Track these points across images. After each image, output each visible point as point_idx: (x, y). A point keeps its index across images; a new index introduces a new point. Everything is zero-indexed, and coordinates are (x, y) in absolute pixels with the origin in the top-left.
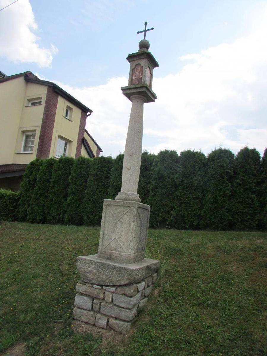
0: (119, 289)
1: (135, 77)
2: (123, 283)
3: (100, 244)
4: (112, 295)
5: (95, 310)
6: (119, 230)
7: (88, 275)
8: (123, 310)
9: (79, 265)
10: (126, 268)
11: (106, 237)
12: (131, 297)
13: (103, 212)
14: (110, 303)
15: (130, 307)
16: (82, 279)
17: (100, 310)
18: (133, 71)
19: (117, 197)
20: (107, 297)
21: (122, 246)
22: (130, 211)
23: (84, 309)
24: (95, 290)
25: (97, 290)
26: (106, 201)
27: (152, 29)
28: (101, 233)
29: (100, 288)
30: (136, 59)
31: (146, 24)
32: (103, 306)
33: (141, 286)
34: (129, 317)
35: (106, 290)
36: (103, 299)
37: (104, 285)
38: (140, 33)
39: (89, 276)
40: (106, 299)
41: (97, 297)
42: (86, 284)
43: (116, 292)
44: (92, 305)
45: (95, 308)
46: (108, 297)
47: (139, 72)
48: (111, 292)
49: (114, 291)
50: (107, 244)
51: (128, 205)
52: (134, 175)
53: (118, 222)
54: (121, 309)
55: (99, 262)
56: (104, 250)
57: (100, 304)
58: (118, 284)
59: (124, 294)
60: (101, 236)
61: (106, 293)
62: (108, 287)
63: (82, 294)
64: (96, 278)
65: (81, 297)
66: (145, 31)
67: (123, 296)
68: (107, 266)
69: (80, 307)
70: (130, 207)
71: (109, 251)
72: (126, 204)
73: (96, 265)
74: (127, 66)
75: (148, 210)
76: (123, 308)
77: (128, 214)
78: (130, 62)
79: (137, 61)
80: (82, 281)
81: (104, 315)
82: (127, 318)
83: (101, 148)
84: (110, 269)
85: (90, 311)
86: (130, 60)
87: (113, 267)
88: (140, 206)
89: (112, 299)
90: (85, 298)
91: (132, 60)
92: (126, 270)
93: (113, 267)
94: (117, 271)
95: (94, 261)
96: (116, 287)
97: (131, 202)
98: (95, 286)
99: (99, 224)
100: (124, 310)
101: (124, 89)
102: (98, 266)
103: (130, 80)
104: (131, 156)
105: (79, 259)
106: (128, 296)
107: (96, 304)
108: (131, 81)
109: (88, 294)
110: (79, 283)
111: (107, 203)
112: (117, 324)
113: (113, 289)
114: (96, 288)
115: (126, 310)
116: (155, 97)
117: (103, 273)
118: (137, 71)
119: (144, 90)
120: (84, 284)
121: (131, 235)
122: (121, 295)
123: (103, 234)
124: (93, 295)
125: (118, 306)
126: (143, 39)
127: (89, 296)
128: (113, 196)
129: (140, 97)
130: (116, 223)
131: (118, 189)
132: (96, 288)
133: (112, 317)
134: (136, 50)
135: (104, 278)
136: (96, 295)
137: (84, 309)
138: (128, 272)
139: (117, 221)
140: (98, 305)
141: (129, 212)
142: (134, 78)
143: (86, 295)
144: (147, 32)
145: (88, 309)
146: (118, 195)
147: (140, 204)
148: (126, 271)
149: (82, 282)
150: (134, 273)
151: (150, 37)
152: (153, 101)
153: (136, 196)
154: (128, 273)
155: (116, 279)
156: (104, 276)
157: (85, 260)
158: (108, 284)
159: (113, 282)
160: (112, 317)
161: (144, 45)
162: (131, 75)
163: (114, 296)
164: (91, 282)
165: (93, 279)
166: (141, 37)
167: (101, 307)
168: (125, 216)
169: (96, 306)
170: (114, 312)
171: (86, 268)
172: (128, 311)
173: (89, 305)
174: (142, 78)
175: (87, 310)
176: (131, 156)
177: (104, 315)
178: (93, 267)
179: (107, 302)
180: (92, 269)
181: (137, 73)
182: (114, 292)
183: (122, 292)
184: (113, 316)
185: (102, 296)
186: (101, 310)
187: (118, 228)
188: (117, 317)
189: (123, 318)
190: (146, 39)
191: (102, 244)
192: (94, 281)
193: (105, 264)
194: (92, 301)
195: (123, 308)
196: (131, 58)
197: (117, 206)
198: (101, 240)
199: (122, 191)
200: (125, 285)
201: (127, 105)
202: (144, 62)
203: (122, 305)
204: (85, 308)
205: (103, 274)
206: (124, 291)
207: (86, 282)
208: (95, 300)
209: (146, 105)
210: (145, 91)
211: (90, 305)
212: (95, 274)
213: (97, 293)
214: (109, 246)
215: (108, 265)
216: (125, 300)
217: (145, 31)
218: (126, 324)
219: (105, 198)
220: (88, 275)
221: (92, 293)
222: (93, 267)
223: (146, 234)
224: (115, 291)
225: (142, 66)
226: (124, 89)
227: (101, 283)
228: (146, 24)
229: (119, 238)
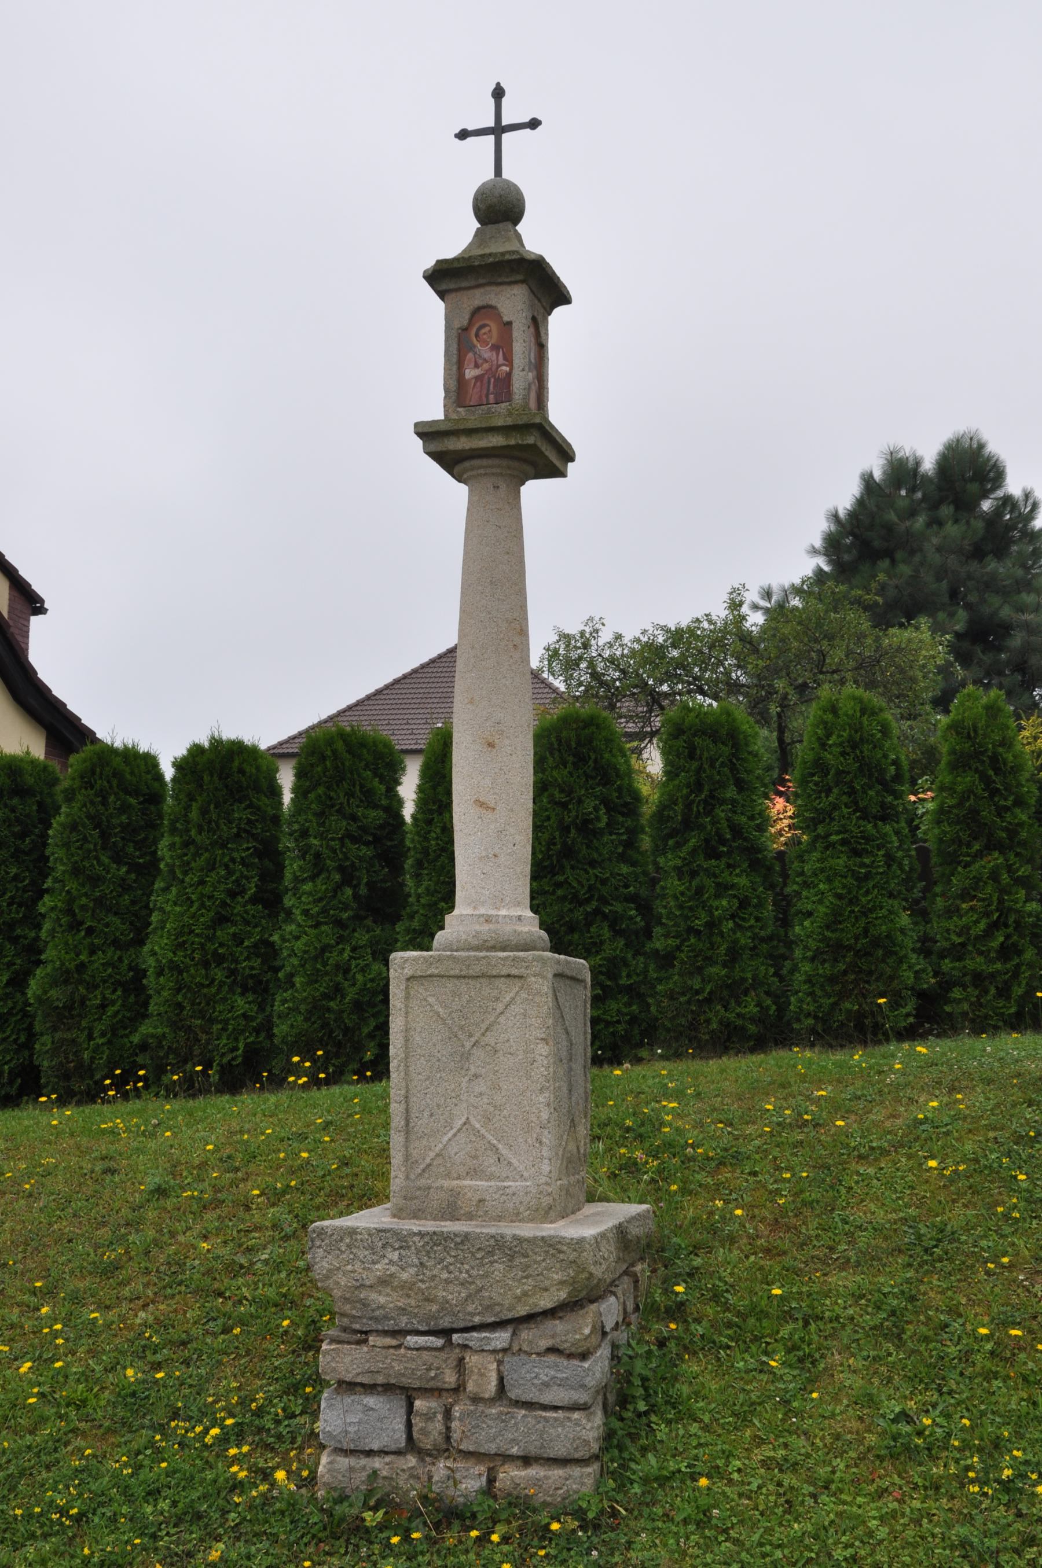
0: (526, 1334)
1: (477, 372)
2: (546, 1302)
3: (397, 1157)
4: (500, 1363)
5: (427, 1444)
6: (480, 1086)
7: (373, 1296)
8: (556, 1419)
9: (322, 1262)
10: (551, 1237)
11: (421, 1123)
12: (584, 1356)
13: (392, 1011)
14: (492, 1401)
15: (583, 1397)
16: (346, 1321)
17: (448, 1438)
18: (460, 344)
19: (440, 936)
20: (475, 1377)
21: (504, 1152)
22: (524, 995)
23: (369, 1453)
24: (416, 1358)
25: (425, 1355)
26: (404, 962)
27: (534, 124)
28: (396, 1109)
29: (439, 1342)
30: (473, 283)
31: (498, 93)
32: (460, 1420)
33: (610, 1310)
34: (587, 1443)
35: (465, 1347)
36: (458, 1389)
37: (455, 1326)
38: (469, 139)
39: (382, 1300)
40: (470, 1387)
41: (431, 1384)
42: (366, 1341)
43: (515, 1348)
44: (409, 1425)
45: (424, 1431)
46: (482, 1375)
47: (495, 348)
48: (494, 1351)
49: (505, 1345)
50: (432, 1154)
51: (514, 971)
52: (512, 831)
53: (474, 1051)
54: (544, 1414)
55: (421, 1235)
56: (422, 1182)
57: (448, 1414)
58: (522, 1311)
59: (552, 1350)
60: (397, 1120)
61: (472, 1360)
62: (475, 1334)
63: (348, 1387)
64: (413, 1303)
65: (348, 1400)
66: (498, 130)
67: (552, 1358)
68: (462, 1242)
69: (352, 1447)
70: (521, 977)
71: (447, 1183)
72: (488, 965)
73: (409, 1247)
74: (431, 312)
75: (583, 981)
76: (556, 1408)
77: (516, 1009)
78: (442, 295)
79: (478, 292)
80: (345, 1329)
81: (468, 1455)
82: (576, 1449)
83: (38, 587)
84: (479, 1256)
85: (398, 1453)
86: (444, 287)
87: (492, 1242)
88: (560, 969)
89: (501, 1380)
90: (371, 1401)
91: (452, 286)
92: (552, 1245)
93: (492, 1242)
94: (512, 1258)
95: (395, 1233)
96: (510, 1330)
97: (521, 954)
98: (411, 1340)
99: (379, 1068)
100: (560, 1414)
101: (427, 433)
102: (418, 1252)
103: (453, 385)
104: (491, 745)
105: (321, 1233)
106: (570, 1356)
107: (429, 1417)
108: (457, 390)
109: (380, 1379)
110: (333, 1341)
111: (408, 972)
112: (537, 1482)
113: (501, 1338)
114: (417, 1349)
115: (567, 1414)
116: (567, 455)
117: (445, 1275)
118: (485, 343)
119: (530, 440)
120: (358, 1343)
121: (541, 1099)
122: (538, 1354)
123: (407, 1110)
124: (405, 1381)
125: (529, 1405)
126: (491, 175)
127: (388, 1388)
128: (422, 939)
129: (509, 468)
130: (466, 1056)
131: (445, 896)
132: (417, 1349)
133: (507, 1458)
134: (457, 234)
135: (454, 1295)
136: (420, 1378)
137: (369, 1453)
138: (560, 1252)
139: (468, 1045)
140: (440, 1417)
141: (518, 1000)
142: (470, 373)
143: (370, 1388)
144: (506, 137)
145: (393, 1447)
146: (442, 928)
147: (558, 962)
148: (552, 1252)
149: (345, 1336)
150: (587, 1256)
151: (524, 164)
152: (559, 473)
153: (528, 924)
154: (561, 1256)
155: (509, 1290)
156: (451, 1287)
157: (352, 1232)
158: (477, 1320)
159: (497, 1309)
160: (507, 1458)
161: (499, 208)
162: (455, 359)
163: (506, 1368)
164: (390, 1325)
165: (403, 1310)
166: (475, 166)
167: (453, 1425)
168: (502, 1019)
169: (430, 1426)
170: (519, 1431)
171: (358, 1266)
172: (576, 1415)
173: (394, 1432)
174: (509, 375)
175: (387, 1453)
176: (491, 745)
177: (468, 1455)
178: (395, 1256)
179: (476, 1400)
180: (393, 1269)
181: (485, 352)
182: (504, 1350)
183: (544, 1344)
184: (515, 1451)
185: (450, 1378)
186: (455, 1436)
187: (476, 1076)
188: (533, 1450)
189: (560, 1450)
190: (505, 175)
191: (407, 1157)
192: (404, 1320)
193: (447, 1237)
194: (403, 1411)
195: (556, 1408)
196: (443, 277)
197: (458, 977)
198: (397, 1140)
199: (461, 908)
200: (551, 1313)
201: (447, 499)
202: (512, 302)
203: (547, 1398)
204: (375, 1447)
205: (447, 1282)
206: (553, 1337)
207: (366, 1333)
208: (418, 1403)
209: (534, 492)
210: (534, 447)
211: (399, 1425)
212: (407, 1288)
213: (429, 1369)
214: (440, 1161)
215: (466, 1236)
216: (559, 1375)
217: (498, 130)
218: (576, 1471)
219: (391, 951)
220: (373, 1296)
221: (403, 1375)
222: (395, 1256)
223: (586, 1092)
224: (510, 1344)
225: (506, 319)
226: (427, 433)
227: (445, 1323)
228: (498, 93)
229: (488, 1119)
